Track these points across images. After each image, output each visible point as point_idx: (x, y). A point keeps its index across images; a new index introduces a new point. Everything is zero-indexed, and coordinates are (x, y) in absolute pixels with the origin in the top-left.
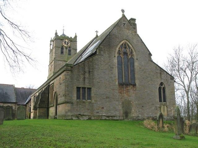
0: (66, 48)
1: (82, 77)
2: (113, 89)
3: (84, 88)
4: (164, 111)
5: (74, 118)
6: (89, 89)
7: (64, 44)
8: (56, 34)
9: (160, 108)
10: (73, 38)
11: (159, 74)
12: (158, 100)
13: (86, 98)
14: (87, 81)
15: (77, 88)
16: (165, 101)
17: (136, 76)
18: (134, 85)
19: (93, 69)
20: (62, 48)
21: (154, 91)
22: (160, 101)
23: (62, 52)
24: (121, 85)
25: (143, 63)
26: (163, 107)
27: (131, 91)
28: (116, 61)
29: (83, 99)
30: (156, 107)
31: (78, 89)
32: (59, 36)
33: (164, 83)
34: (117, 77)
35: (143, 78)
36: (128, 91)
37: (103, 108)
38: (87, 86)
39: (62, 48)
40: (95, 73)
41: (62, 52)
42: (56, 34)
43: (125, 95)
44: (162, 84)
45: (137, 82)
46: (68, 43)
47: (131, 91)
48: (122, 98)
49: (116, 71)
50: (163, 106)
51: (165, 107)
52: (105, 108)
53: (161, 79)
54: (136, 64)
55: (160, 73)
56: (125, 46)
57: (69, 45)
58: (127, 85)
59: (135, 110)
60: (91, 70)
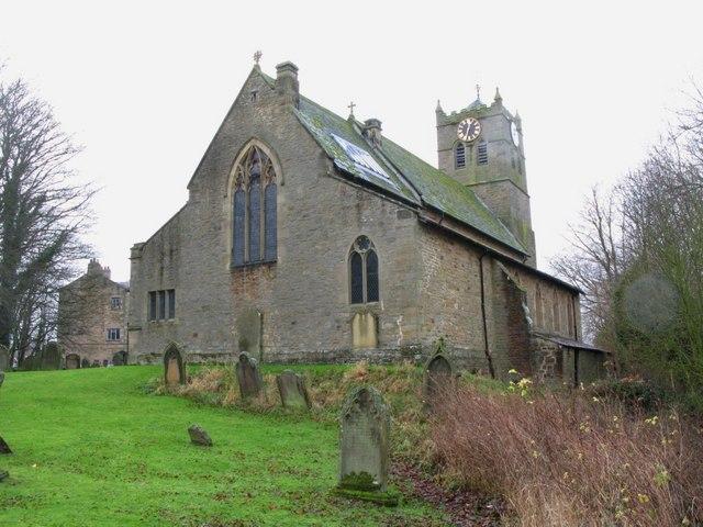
0: (470, 144)
1: (158, 266)
2: (220, 285)
3: (162, 292)
4: (364, 331)
5: (142, 363)
6: (172, 292)
7: (461, 135)
8: (440, 112)
9: (351, 321)
10: (489, 105)
11: (354, 211)
12: (345, 296)
13: (167, 314)
14: (166, 275)
15: (153, 294)
16: (374, 296)
17: (280, 235)
18: (272, 264)
19: (178, 243)
20: (460, 149)
21: (331, 270)
22: (356, 297)
23: (460, 162)
24: (237, 269)
25: (300, 190)
26: (361, 319)
27: (263, 281)
28: (227, 207)
29: (369, 301)
30: (337, 321)
31: (153, 294)
32: (449, 114)
33: (370, 237)
34: (229, 252)
35: (298, 236)
36: (254, 283)
37: (196, 335)
38: (166, 287)
39: (460, 149)
40: (183, 251)
41: (460, 162)
42: (440, 112)
43: (247, 296)
44: (363, 241)
45: (281, 255)
46: (473, 127)
47: (263, 281)
48: (237, 306)
49: (227, 236)
50: (361, 315)
51: (366, 321)
52: (201, 335)
53: (360, 224)
54: (280, 199)
55: (358, 206)
56: (253, 157)
57: (476, 132)
58: (251, 266)
59: (271, 335)
60: (175, 247)
